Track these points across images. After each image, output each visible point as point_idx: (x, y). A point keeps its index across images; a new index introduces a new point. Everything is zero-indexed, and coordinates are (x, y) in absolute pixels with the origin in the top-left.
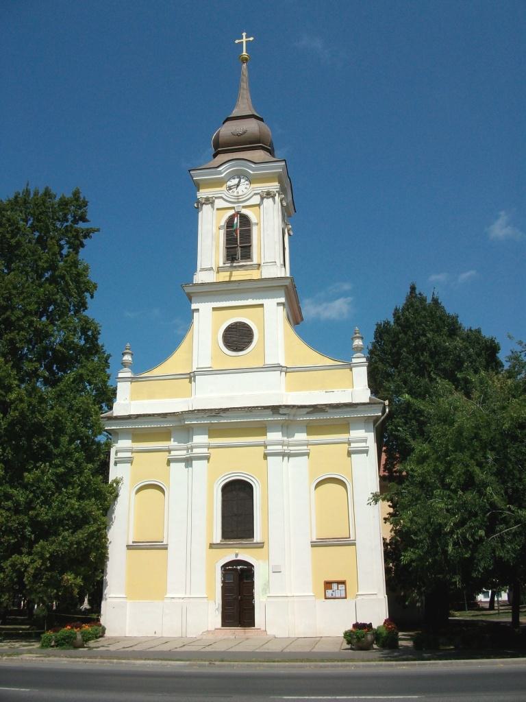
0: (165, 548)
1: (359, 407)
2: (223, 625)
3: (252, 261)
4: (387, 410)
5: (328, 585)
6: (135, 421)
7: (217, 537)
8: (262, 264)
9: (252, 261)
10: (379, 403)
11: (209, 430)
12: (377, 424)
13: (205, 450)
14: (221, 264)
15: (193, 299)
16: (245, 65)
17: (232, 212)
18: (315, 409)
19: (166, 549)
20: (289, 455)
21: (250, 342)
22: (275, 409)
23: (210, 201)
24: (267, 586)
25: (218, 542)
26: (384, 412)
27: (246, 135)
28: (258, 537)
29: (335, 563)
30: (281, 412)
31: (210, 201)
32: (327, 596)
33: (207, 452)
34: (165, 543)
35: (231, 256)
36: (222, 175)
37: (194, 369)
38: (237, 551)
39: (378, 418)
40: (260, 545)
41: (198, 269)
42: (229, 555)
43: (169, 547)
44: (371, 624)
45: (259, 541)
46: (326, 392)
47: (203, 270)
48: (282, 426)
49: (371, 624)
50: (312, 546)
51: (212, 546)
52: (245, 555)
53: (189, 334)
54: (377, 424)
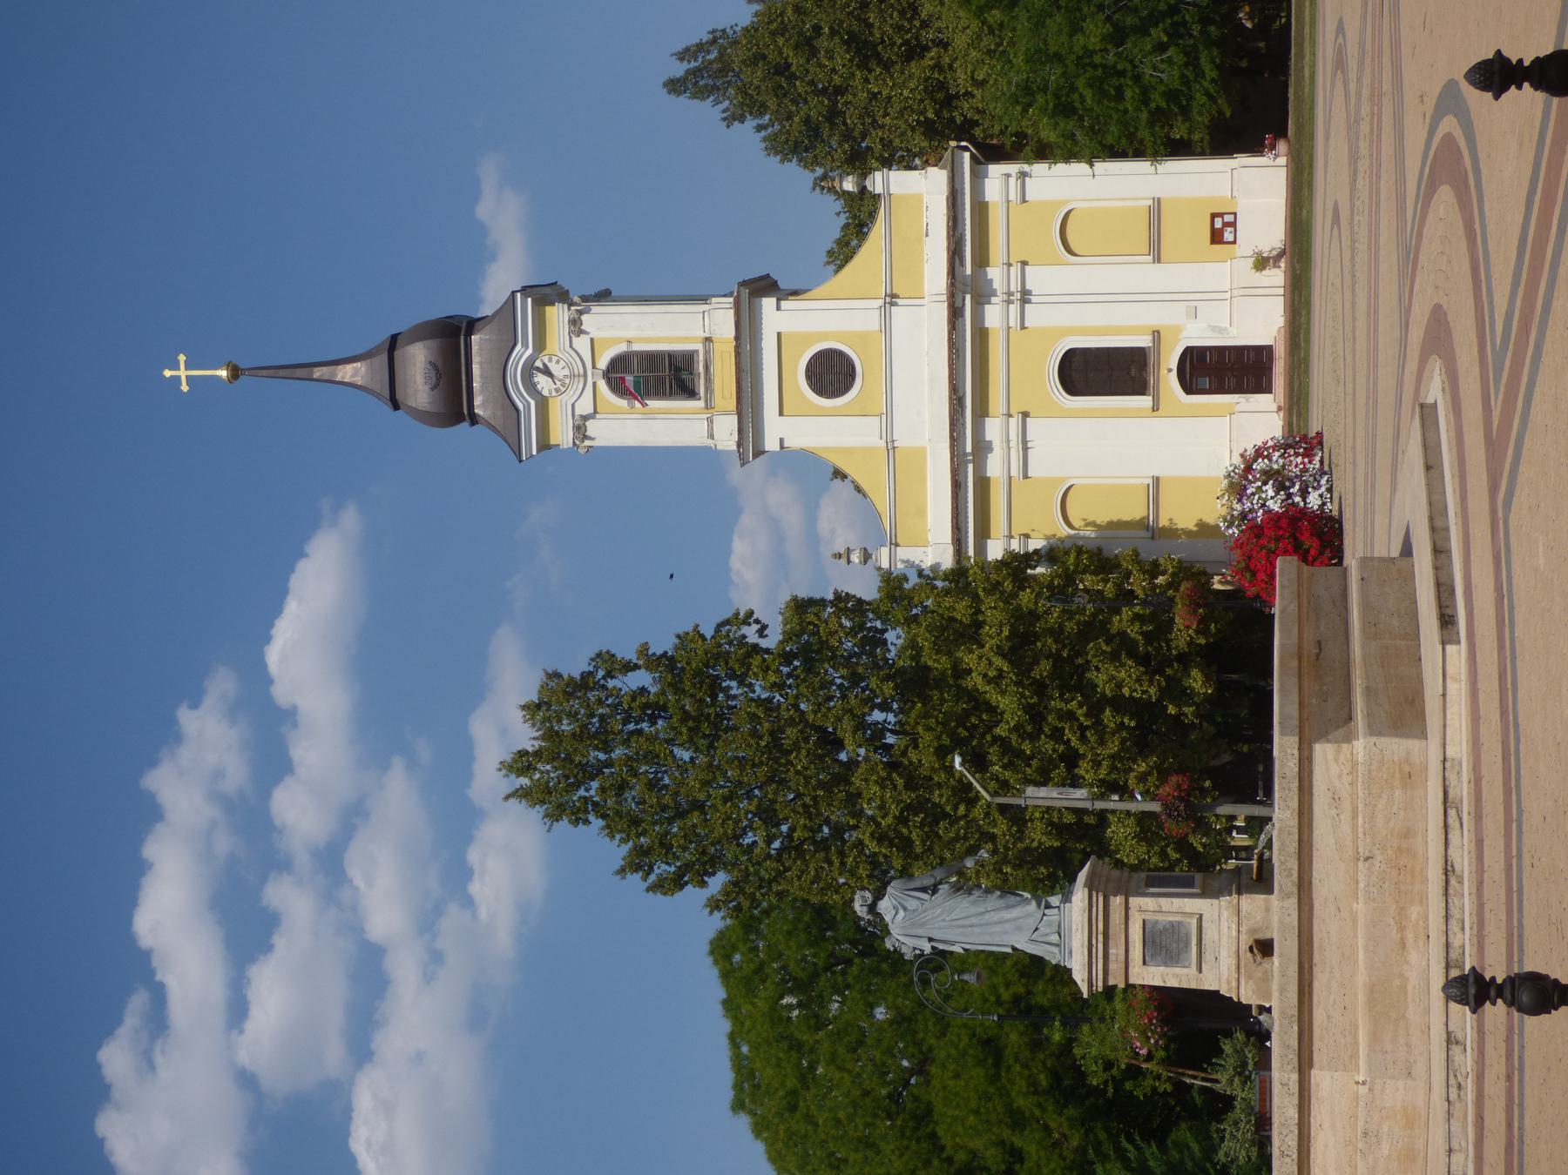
0: (1156, 480)
1: (956, 186)
2: (1271, 392)
3: (697, 351)
4: (964, 144)
5: (1216, 239)
6: (963, 533)
7: (1145, 401)
8: (707, 335)
9: (697, 351)
10: (953, 154)
11: (981, 417)
12: (980, 157)
13: (1013, 421)
14: (701, 404)
15: (761, 449)
16: (223, 373)
17: (602, 385)
18: (955, 253)
19: (1158, 478)
20: (1025, 442)
21: (841, 354)
22: (955, 313)
23: (580, 430)
24: (1220, 331)
25: (1151, 398)
26: (966, 149)
27: (440, 364)
28: (1143, 341)
29: (1189, 230)
30: (960, 305)
31: (580, 430)
32: (1231, 239)
33: (1017, 540)
34: (1150, 481)
35: (686, 390)
36: (533, 403)
37: (882, 443)
38: (1163, 371)
39: (973, 157)
40: (1156, 334)
41: (710, 443)
42: (1170, 381)
43: (1157, 474)
44: (1499, 52)
45: (1150, 338)
46: (927, 235)
47: (711, 436)
48: (980, 304)
49: (1499, 52)
50: (1159, 262)
51: (1155, 408)
52: (1171, 359)
53: (826, 455)
54: (980, 157)
